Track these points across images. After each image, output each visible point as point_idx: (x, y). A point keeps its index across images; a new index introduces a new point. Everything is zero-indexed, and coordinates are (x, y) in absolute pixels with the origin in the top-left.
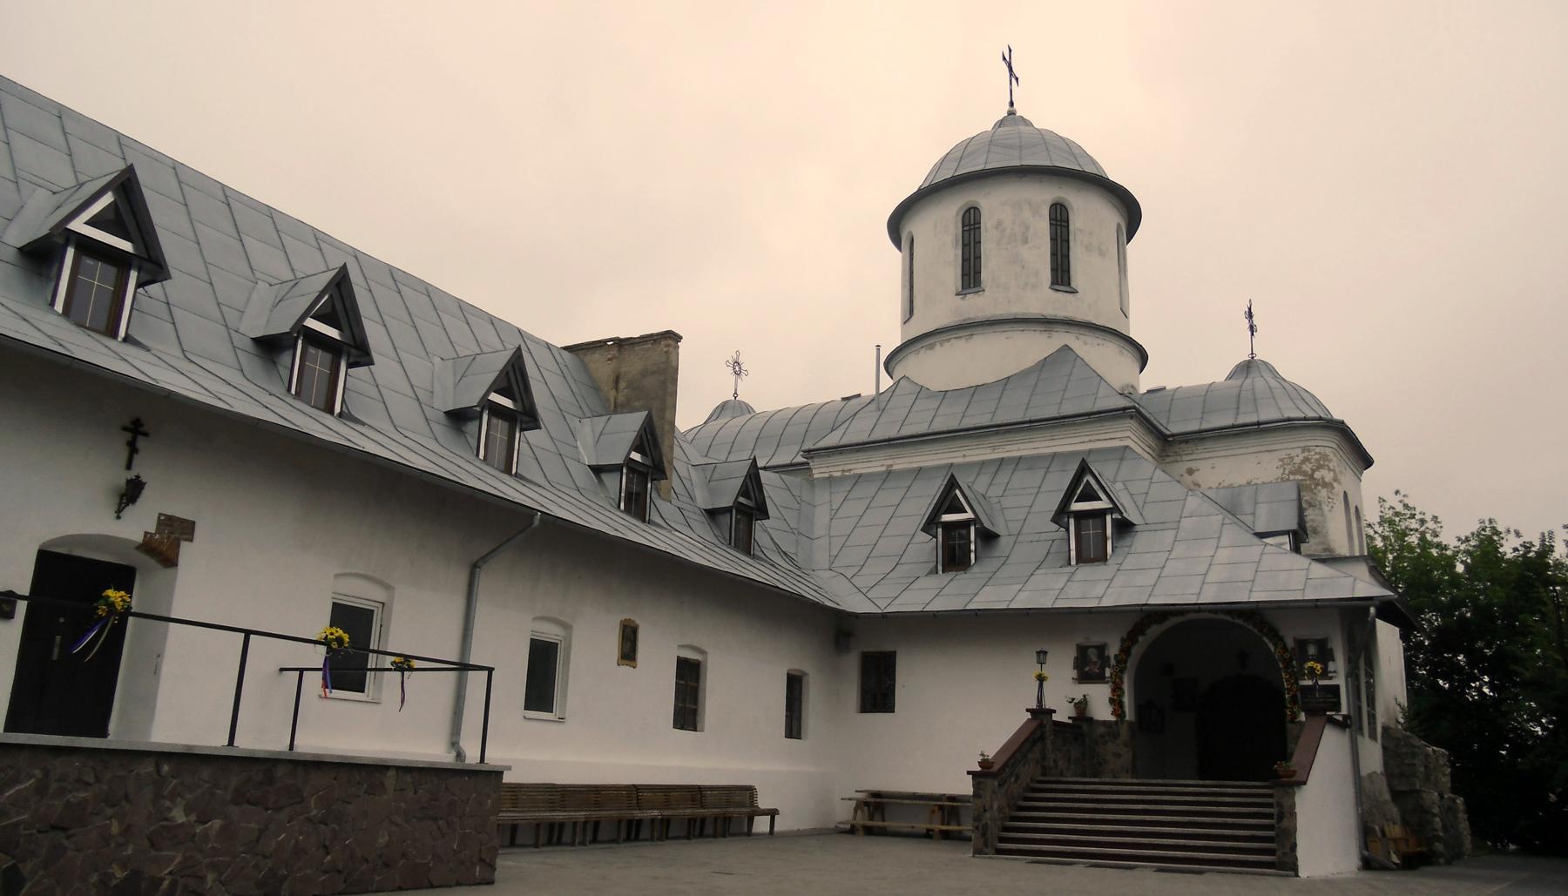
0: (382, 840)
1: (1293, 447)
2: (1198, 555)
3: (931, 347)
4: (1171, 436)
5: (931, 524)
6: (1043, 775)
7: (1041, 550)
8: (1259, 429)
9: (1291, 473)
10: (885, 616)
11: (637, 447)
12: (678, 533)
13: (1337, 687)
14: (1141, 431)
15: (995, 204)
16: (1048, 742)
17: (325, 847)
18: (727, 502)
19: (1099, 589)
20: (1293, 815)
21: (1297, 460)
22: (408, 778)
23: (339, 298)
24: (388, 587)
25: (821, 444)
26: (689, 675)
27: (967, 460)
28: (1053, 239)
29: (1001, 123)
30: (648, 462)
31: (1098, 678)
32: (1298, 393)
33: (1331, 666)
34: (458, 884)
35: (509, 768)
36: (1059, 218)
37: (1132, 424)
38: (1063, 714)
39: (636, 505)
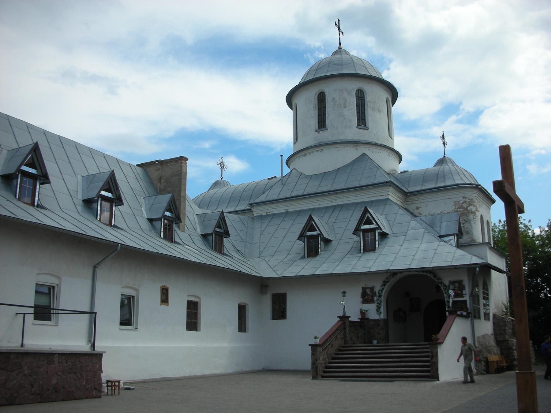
0: (54, 382)
1: (458, 196)
2: (415, 248)
3: (305, 155)
4: (413, 191)
5: (301, 237)
6: (345, 343)
7: (348, 247)
8: (445, 189)
9: (459, 208)
10: (280, 278)
11: (169, 210)
12: (189, 246)
13: (465, 301)
14: (395, 192)
15: (331, 90)
16: (347, 330)
17: (32, 385)
18: (210, 231)
19: (370, 264)
20: (437, 356)
21: (461, 202)
22: (64, 357)
23: (35, 156)
24: (59, 278)
25: (257, 201)
26: (193, 309)
27: (320, 206)
28: (358, 106)
29: (335, 53)
30: (174, 216)
31: (372, 301)
32: (462, 172)
33: (464, 292)
34: (86, 398)
35: (105, 352)
36: (361, 97)
37: (391, 189)
38: (355, 317)
39: (169, 236)
